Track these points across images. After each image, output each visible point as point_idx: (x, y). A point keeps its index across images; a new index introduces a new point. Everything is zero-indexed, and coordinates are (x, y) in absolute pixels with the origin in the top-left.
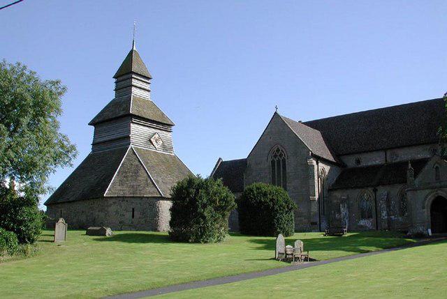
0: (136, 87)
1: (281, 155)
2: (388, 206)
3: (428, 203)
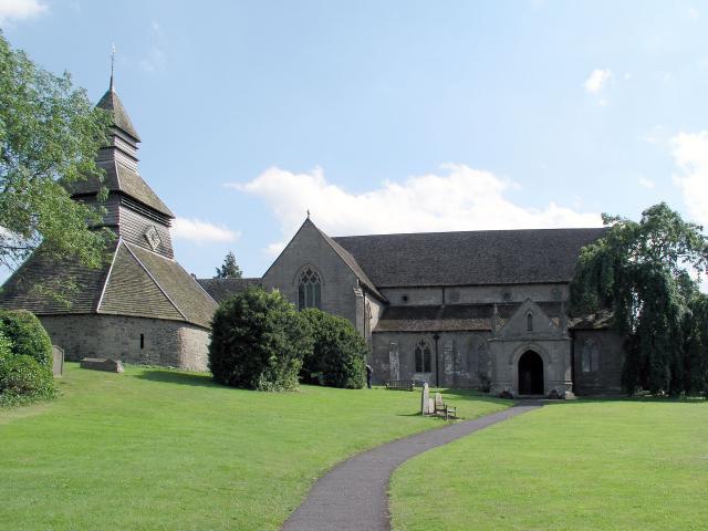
0: (119, 150)
1: (314, 279)
3: (516, 358)
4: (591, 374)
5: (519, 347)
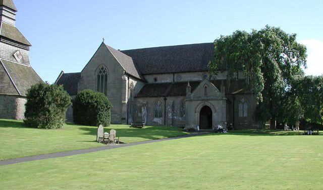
0: (4, 16)
1: (104, 72)
2: (173, 110)
3: (199, 109)
4: (243, 118)
5: (200, 103)
